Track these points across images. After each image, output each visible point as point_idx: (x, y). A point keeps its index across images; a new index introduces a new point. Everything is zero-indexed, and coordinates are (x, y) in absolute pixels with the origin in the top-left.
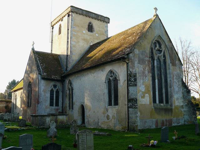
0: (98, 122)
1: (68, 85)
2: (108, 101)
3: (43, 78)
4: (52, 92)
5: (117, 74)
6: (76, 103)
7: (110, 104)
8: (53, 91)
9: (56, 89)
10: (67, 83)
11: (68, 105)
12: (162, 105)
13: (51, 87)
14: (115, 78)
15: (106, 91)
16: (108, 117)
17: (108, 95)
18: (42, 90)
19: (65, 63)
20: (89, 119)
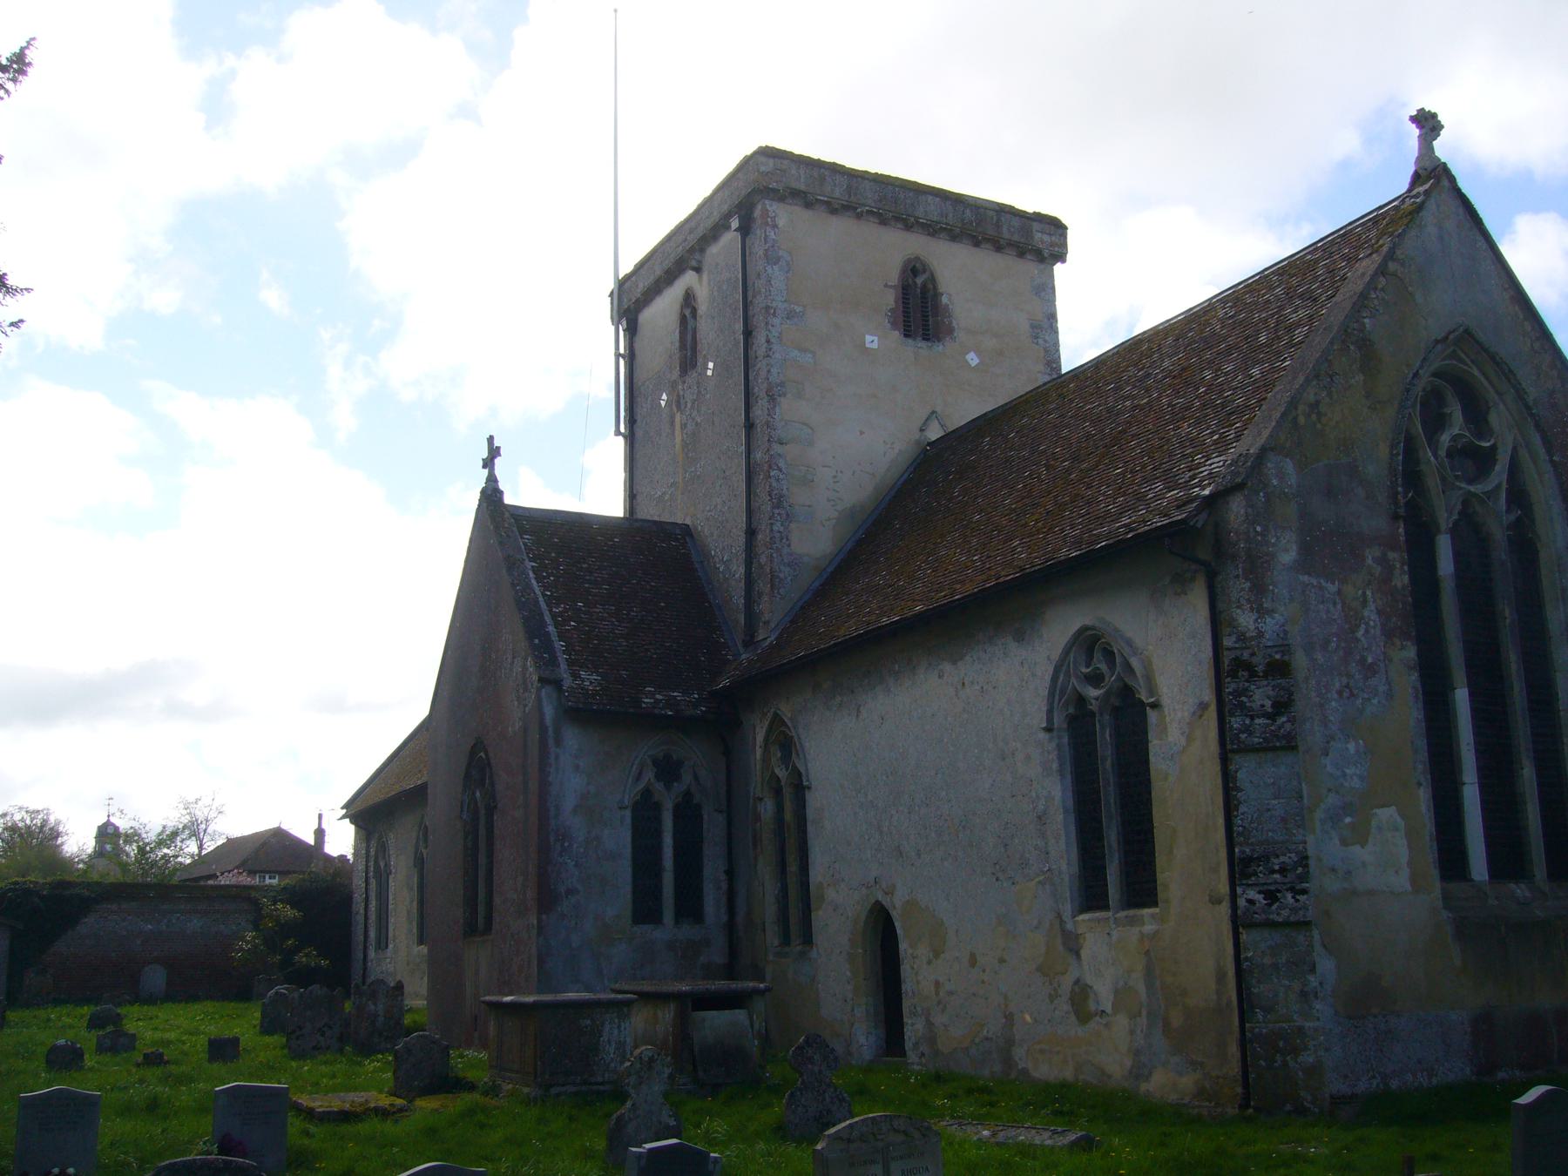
0: (1010, 1042)
1: (766, 759)
2: (1075, 869)
3: (581, 713)
4: (644, 813)
5: (1134, 662)
6: (831, 894)
7: (1092, 896)
8: (657, 807)
9: (678, 788)
10: (760, 738)
11: (770, 911)
12: (1520, 890)
13: (638, 778)
14: (1127, 692)
15: (1055, 792)
16: (1080, 997)
17: (1072, 828)
18: (569, 803)
19: (739, 600)
20: (939, 1019)
